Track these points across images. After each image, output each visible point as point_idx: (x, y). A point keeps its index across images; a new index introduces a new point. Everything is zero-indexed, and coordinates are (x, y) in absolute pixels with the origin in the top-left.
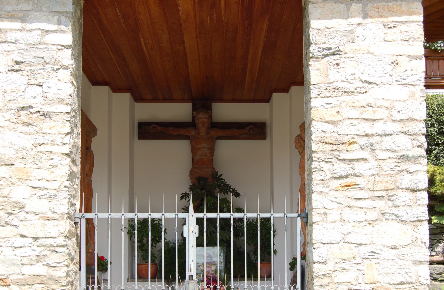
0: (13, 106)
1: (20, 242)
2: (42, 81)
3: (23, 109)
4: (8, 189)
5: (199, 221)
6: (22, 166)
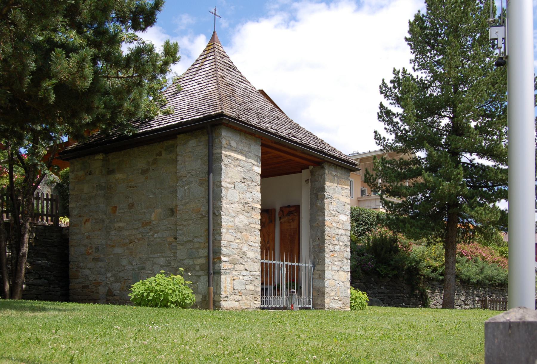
0: (243, 201)
1: (245, 273)
2: (252, 190)
3: (246, 203)
4: (241, 245)
5: (287, 266)
6: (245, 233)
